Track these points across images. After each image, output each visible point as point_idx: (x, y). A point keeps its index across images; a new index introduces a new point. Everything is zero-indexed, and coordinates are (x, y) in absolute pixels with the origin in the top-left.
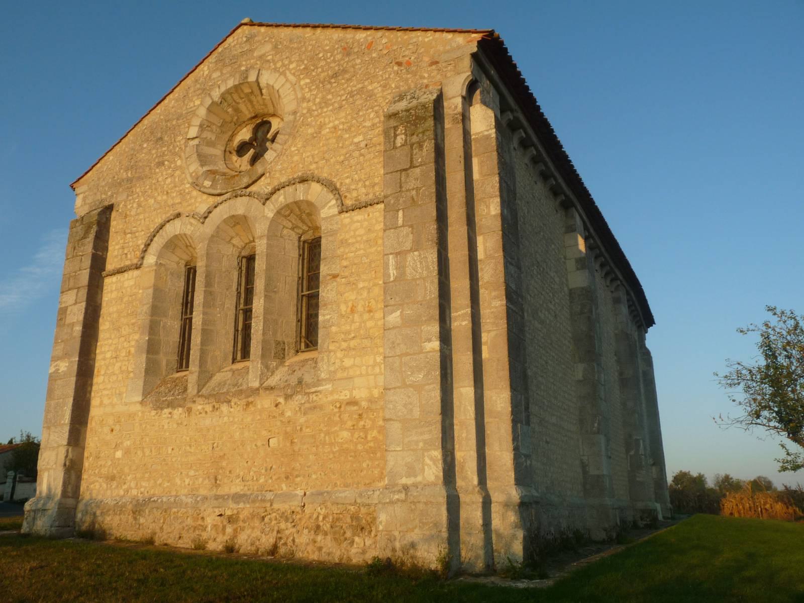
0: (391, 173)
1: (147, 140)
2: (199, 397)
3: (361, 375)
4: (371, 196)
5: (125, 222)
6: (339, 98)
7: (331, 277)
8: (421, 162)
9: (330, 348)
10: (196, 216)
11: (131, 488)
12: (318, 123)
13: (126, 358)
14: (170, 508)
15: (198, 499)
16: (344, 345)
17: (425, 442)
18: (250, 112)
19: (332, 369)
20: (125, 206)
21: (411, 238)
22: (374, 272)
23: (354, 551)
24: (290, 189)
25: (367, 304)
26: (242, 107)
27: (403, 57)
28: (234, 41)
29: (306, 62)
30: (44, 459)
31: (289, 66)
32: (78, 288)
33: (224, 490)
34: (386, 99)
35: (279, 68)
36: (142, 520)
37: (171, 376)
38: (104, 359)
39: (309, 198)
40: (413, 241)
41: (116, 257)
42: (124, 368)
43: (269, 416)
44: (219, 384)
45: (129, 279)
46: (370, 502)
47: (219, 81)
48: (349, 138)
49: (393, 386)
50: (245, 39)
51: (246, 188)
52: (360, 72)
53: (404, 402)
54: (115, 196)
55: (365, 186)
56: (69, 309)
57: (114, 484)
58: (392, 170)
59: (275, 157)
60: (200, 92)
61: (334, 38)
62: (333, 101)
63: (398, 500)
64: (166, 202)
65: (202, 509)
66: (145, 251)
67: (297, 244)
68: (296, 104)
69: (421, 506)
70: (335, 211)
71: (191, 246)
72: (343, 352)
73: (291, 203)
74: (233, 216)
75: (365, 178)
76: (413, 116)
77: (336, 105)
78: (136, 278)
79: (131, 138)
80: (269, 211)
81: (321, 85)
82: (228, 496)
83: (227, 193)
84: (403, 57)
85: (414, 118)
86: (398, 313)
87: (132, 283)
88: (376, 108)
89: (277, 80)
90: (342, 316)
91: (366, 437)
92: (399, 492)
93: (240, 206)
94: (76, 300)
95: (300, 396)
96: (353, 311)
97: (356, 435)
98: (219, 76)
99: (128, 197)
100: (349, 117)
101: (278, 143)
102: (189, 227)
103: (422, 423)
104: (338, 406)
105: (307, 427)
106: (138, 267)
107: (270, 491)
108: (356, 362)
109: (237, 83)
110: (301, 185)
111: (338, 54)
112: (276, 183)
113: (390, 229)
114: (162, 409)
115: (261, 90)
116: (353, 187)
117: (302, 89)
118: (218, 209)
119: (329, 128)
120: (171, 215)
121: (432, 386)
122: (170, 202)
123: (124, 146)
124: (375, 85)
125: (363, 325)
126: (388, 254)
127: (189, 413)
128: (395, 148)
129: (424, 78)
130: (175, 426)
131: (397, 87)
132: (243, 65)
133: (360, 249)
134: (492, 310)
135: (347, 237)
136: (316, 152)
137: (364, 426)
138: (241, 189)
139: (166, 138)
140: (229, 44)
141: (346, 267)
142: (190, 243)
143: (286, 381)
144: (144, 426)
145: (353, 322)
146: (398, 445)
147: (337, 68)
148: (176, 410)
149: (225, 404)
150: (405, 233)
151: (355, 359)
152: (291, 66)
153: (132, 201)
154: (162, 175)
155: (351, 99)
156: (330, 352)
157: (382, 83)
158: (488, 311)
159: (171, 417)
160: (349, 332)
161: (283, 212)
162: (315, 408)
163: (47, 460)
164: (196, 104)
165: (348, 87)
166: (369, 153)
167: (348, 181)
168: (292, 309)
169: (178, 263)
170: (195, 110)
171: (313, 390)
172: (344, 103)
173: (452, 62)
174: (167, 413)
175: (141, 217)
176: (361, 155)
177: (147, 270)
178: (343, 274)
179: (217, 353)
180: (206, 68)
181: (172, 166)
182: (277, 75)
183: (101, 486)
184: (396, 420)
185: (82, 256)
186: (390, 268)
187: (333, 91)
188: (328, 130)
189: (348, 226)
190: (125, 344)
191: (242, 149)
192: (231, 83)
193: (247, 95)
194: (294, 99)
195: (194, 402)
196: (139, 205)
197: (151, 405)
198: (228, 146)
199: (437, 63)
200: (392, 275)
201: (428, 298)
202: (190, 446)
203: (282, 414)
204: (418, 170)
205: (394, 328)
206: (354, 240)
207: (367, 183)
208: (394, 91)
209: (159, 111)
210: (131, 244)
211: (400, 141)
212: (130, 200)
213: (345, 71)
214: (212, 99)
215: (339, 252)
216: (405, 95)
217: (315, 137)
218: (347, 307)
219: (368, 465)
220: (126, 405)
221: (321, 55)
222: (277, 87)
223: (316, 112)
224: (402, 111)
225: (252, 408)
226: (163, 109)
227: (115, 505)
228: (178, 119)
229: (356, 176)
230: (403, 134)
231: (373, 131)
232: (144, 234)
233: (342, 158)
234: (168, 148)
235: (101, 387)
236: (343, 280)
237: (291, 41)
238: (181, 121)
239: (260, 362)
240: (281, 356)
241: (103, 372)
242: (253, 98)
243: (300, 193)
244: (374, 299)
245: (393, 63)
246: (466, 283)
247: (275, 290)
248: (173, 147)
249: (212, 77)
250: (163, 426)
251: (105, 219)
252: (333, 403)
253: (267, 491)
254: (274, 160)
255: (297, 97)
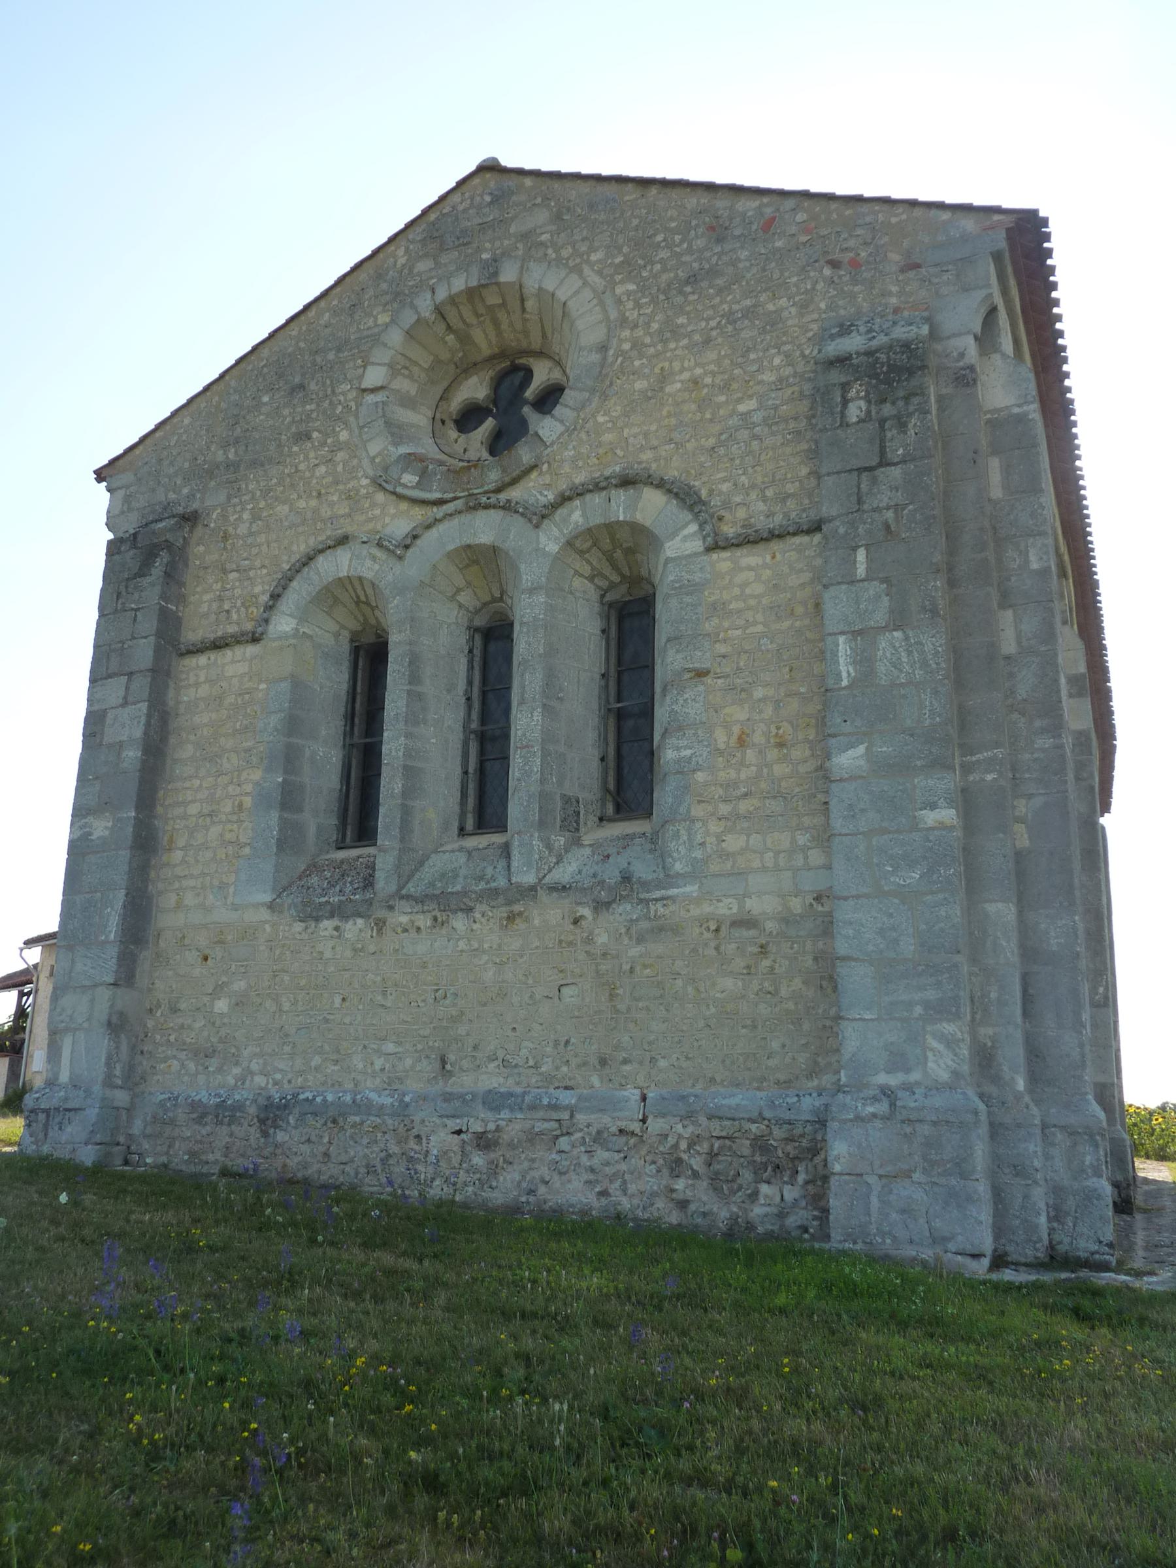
0: (838, 473)
1: (270, 389)
2: (402, 897)
3: (764, 869)
4: (778, 519)
5: (225, 548)
6: (703, 324)
7: (692, 674)
8: (904, 455)
9: (693, 813)
10: (385, 543)
11: (252, 1073)
12: (657, 370)
13: (235, 818)
14: (344, 1115)
15: (407, 1099)
16: (724, 809)
17: (927, 1005)
18: (490, 343)
19: (698, 854)
20: (225, 517)
21: (887, 604)
22: (787, 669)
23: (757, 1211)
24: (597, 499)
25: (774, 731)
26: (478, 335)
27: (842, 250)
28: (462, 201)
29: (625, 250)
30: (63, 1010)
31: (589, 257)
32: (130, 674)
33: (465, 1082)
34: (807, 331)
35: (568, 259)
36: (281, 1136)
37: (327, 857)
38: (185, 817)
39: (639, 517)
40: (891, 612)
41: (206, 615)
42: (228, 836)
43: (561, 942)
44: (443, 875)
45: (235, 664)
46: (792, 1117)
47: (432, 278)
48: (727, 402)
49: (854, 893)
50: (488, 199)
51: (498, 490)
52: (749, 275)
53: (879, 925)
54: (198, 496)
55: (765, 499)
56: (110, 715)
57: (213, 1063)
58: (839, 468)
59: (562, 434)
60: (388, 297)
61: (689, 206)
62: (689, 329)
63: (874, 1115)
64: (315, 511)
65: (417, 1119)
66: (269, 608)
67: (597, 607)
68: (605, 330)
69: (925, 1130)
70: (697, 545)
71: (367, 603)
72: (723, 823)
73: (598, 526)
74: (469, 546)
75: (763, 483)
76: (883, 364)
77: (697, 337)
78: (251, 660)
79: (233, 383)
80: (550, 540)
81: (662, 297)
82: (474, 1096)
83: (456, 498)
84: (842, 250)
85: (885, 369)
86: (861, 749)
87: (242, 668)
88: (787, 347)
89: (562, 282)
90: (721, 753)
91: (777, 991)
92: (875, 1099)
93: (484, 528)
94: (125, 698)
95: (629, 907)
96: (742, 742)
97: (755, 985)
98: (431, 270)
99: (229, 498)
100: (727, 362)
101: (566, 406)
102: (368, 563)
103: (920, 968)
104: (713, 928)
105: (645, 966)
106: (255, 639)
107: (566, 1088)
108: (751, 842)
109: (474, 283)
110: (621, 491)
111: (697, 237)
112: (563, 486)
113: (839, 583)
114: (317, 919)
115: (522, 300)
116: (738, 499)
117: (619, 302)
118: (434, 530)
119: (682, 382)
120: (328, 538)
121: (941, 896)
122: (326, 512)
123: (217, 398)
124: (783, 302)
125: (765, 770)
126: (835, 634)
127: (380, 931)
128: (845, 425)
129: (890, 294)
130: (349, 953)
131: (829, 308)
132: (486, 250)
133: (755, 623)
134: (1036, 755)
135: (726, 596)
136: (654, 428)
137: (772, 968)
138: (486, 492)
139: (313, 386)
140: (454, 208)
141: (724, 657)
142: (366, 596)
143: (595, 876)
144: (278, 952)
145: (742, 763)
146: (868, 1009)
147: (696, 265)
148: (351, 922)
149: (459, 914)
150: (871, 592)
151: (748, 836)
152: (593, 257)
153: (238, 508)
154: (307, 458)
155: (730, 328)
156: (693, 821)
157: (797, 299)
158: (1027, 756)
159: (339, 937)
160: (735, 784)
161: (578, 544)
162: (661, 929)
163: (69, 1012)
164: (379, 322)
165: (721, 303)
166: (773, 434)
167: (725, 487)
168: (590, 736)
169: (337, 635)
170: (379, 334)
171: (657, 894)
172: (714, 333)
173: (950, 267)
174: (330, 929)
175: (261, 539)
176: (755, 437)
177: (276, 644)
178: (718, 671)
179: (431, 814)
180: (401, 252)
181: (329, 441)
182: (563, 273)
183: (183, 1066)
184: (863, 961)
185: (138, 609)
186: (841, 660)
187: (688, 309)
188: (679, 385)
189: (728, 578)
190: (230, 788)
191: (468, 418)
192: (459, 284)
193: (491, 309)
194: (600, 322)
195: (391, 908)
196: (256, 517)
197: (293, 912)
198: (440, 409)
199: (917, 266)
200: (844, 675)
201: (927, 723)
202: (384, 993)
203: (589, 940)
204: (896, 472)
205: (853, 778)
206: (741, 605)
207: (769, 493)
208: (824, 316)
209: (294, 333)
210: (238, 592)
211: (855, 411)
212: (234, 506)
213: (714, 273)
214: (418, 313)
215: (708, 627)
216: (852, 325)
217: (650, 398)
218: (729, 735)
219: (784, 1046)
220: (236, 910)
221: (659, 238)
222: (562, 295)
223: (652, 350)
224: (858, 353)
225: (520, 925)
226: (304, 328)
227: (218, 1106)
228: (339, 350)
229: (743, 478)
230: (861, 398)
231: (780, 393)
232: (268, 574)
233: (712, 441)
234: (318, 405)
235: (179, 871)
236: (720, 681)
237: (592, 207)
238: (346, 354)
239: (536, 835)
240: (572, 823)
241: (181, 843)
242: (502, 316)
243: (620, 507)
244: (791, 723)
245: (822, 262)
246: (525, 723)
247: (561, 695)
248: (331, 403)
249: (416, 271)
250: (321, 953)
251: (181, 540)
252: (702, 921)
253: (558, 1088)
254: (559, 438)
255: (607, 318)
